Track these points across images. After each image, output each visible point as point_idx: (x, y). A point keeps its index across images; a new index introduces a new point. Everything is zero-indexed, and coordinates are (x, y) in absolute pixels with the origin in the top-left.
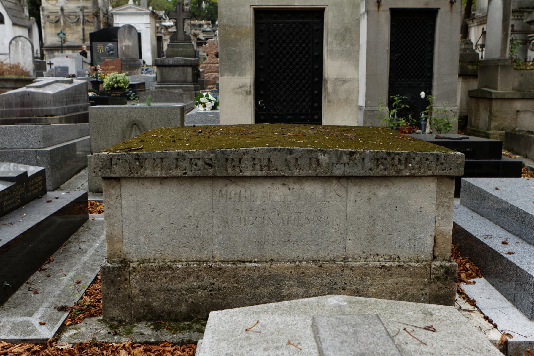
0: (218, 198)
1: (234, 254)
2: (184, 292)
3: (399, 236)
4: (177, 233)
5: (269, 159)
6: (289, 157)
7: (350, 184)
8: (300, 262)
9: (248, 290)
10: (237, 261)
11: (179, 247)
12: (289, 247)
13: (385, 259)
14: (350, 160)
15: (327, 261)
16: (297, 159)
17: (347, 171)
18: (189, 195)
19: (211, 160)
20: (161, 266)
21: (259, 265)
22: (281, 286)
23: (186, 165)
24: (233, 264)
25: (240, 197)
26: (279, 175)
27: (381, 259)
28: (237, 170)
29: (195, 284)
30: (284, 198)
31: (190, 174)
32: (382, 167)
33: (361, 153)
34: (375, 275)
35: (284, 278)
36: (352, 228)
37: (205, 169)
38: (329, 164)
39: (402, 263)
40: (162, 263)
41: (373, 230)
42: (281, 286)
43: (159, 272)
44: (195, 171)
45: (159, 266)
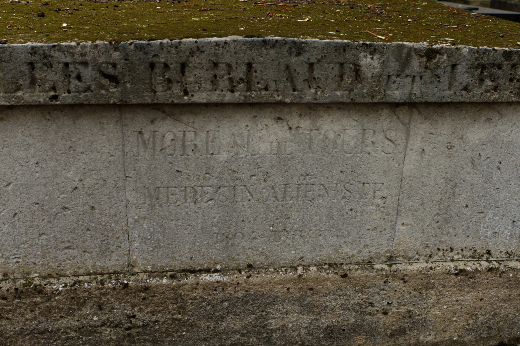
0: (135, 150)
1: (173, 258)
2: (74, 334)
3: (495, 214)
4: (49, 222)
5: (249, 66)
6: (294, 60)
7: (416, 117)
8: (306, 268)
9: (202, 324)
10: (178, 271)
11: (57, 248)
12: (284, 241)
13: (464, 256)
14: (426, 68)
15: (358, 263)
16: (311, 65)
17: (418, 93)
18: (69, 144)
19: (114, 66)
20: (21, 289)
21: (225, 279)
22: (268, 313)
23: (56, 78)
24: (172, 277)
25: (184, 146)
26: (271, 100)
27: (456, 257)
28: (176, 90)
29: (95, 318)
30: (279, 147)
31: (65, 98)
32: (490, 83)
33: (450, 53)
34: (444, 286)
35: (275, 300)
36: (410, 203)
37: (102, 87)
38: (380, 76)
39: (495, 264)
40: (22, 281)
41: (448, 206)
42: (268, 313)
43: (16, 301)
44: (79, 92)
45: (16, 289)
